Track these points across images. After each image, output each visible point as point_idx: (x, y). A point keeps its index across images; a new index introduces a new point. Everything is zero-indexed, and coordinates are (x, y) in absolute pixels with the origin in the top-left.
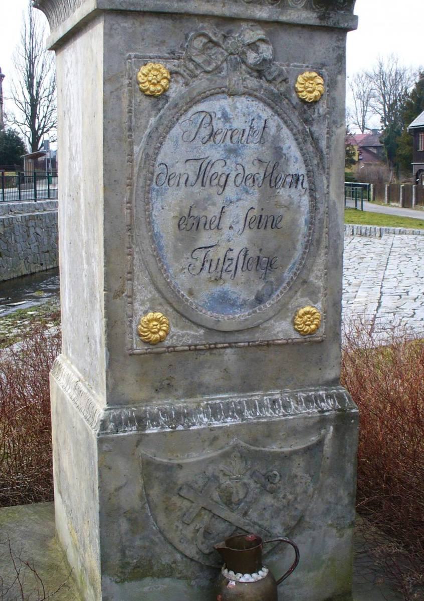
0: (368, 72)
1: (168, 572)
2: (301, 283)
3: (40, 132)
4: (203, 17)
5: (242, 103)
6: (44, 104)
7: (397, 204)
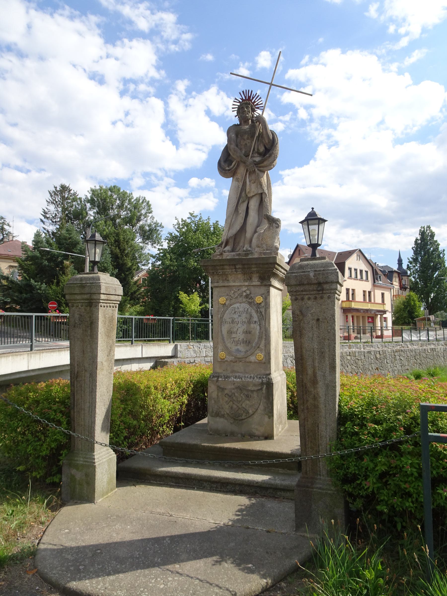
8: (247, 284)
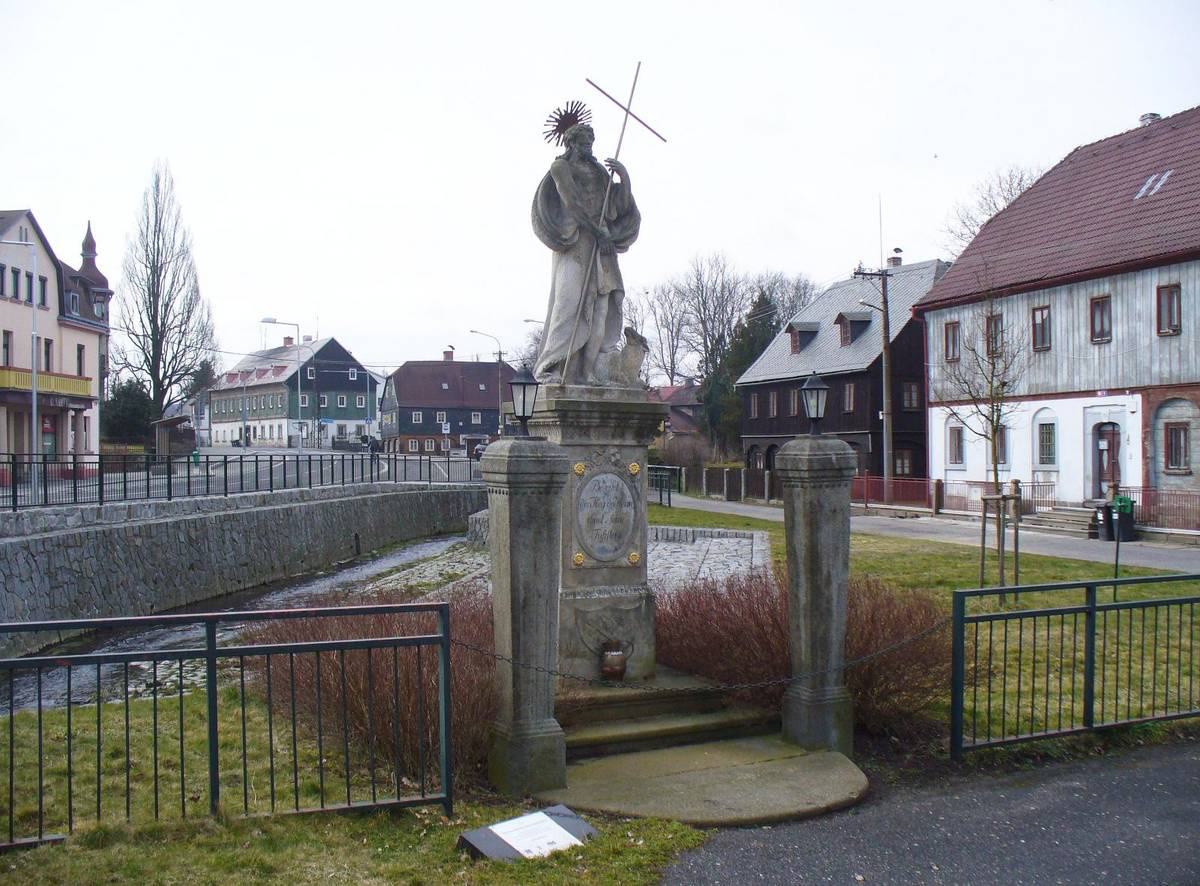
0: (680, 287)
1: (583, 656)
2: (631, 543)
3: (167, 381)
4: (595, 445)
5: (610, 476)
6: (172, 340)
7: (719, 497)
8: (617, 442)
